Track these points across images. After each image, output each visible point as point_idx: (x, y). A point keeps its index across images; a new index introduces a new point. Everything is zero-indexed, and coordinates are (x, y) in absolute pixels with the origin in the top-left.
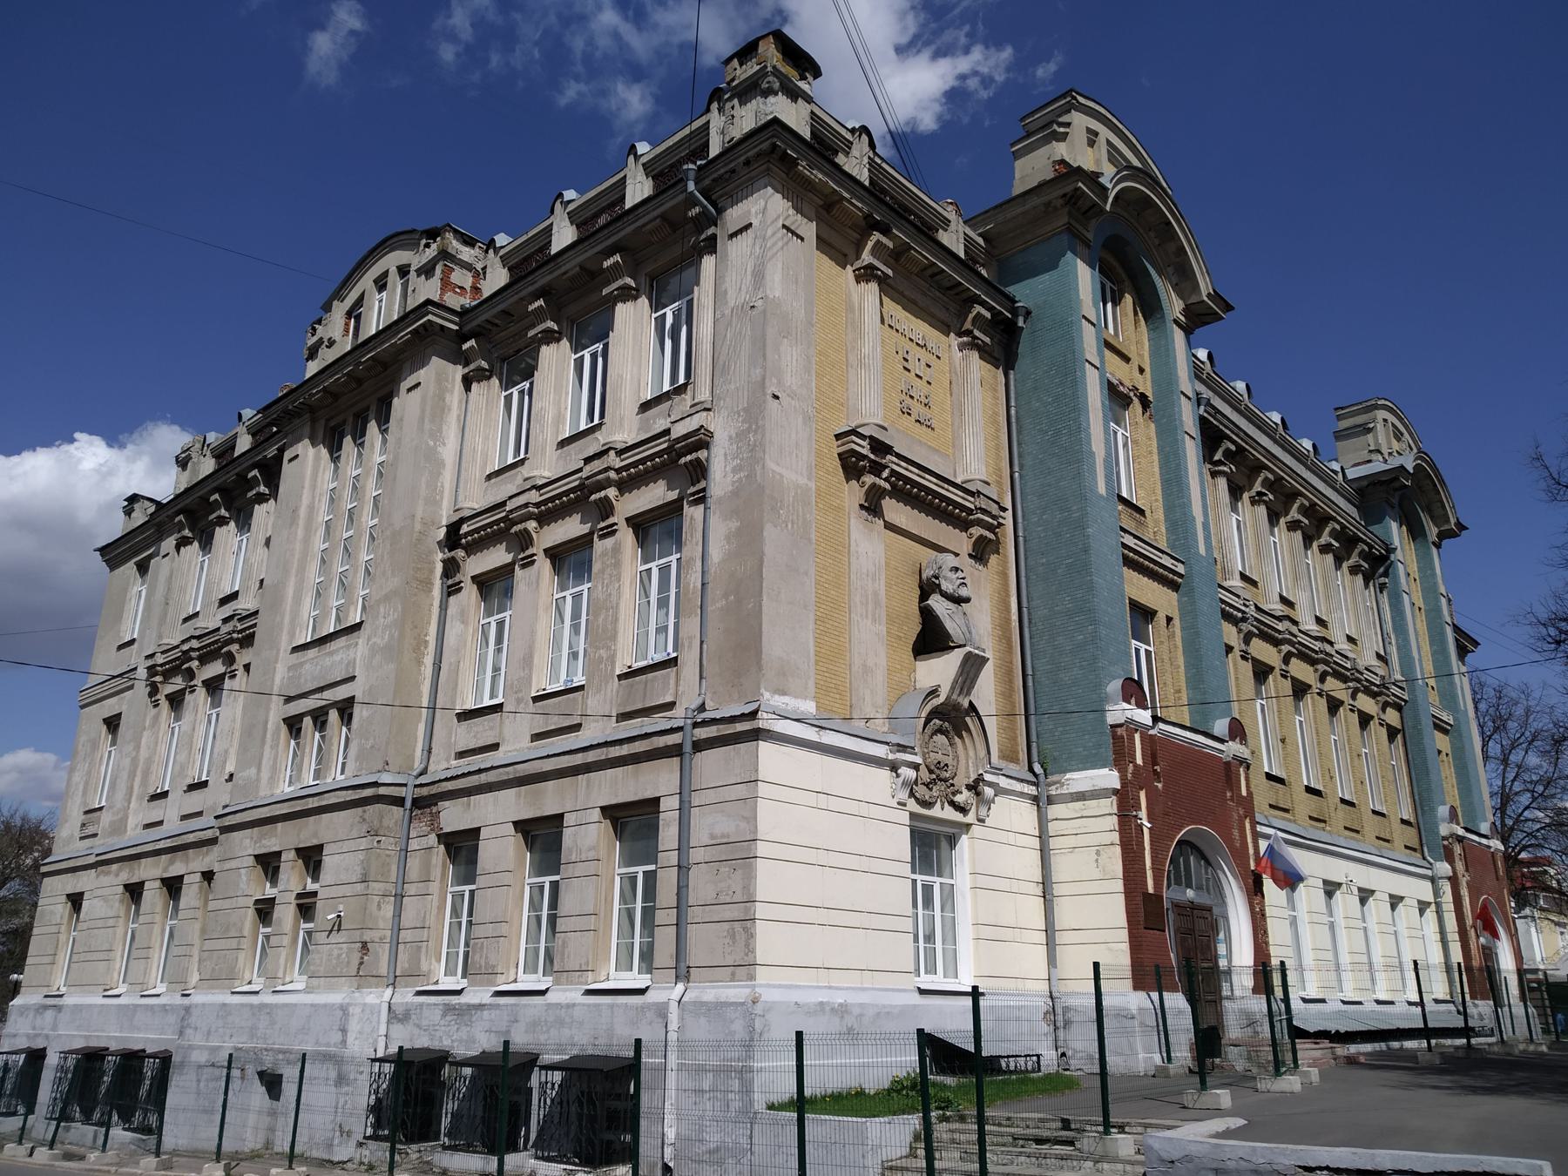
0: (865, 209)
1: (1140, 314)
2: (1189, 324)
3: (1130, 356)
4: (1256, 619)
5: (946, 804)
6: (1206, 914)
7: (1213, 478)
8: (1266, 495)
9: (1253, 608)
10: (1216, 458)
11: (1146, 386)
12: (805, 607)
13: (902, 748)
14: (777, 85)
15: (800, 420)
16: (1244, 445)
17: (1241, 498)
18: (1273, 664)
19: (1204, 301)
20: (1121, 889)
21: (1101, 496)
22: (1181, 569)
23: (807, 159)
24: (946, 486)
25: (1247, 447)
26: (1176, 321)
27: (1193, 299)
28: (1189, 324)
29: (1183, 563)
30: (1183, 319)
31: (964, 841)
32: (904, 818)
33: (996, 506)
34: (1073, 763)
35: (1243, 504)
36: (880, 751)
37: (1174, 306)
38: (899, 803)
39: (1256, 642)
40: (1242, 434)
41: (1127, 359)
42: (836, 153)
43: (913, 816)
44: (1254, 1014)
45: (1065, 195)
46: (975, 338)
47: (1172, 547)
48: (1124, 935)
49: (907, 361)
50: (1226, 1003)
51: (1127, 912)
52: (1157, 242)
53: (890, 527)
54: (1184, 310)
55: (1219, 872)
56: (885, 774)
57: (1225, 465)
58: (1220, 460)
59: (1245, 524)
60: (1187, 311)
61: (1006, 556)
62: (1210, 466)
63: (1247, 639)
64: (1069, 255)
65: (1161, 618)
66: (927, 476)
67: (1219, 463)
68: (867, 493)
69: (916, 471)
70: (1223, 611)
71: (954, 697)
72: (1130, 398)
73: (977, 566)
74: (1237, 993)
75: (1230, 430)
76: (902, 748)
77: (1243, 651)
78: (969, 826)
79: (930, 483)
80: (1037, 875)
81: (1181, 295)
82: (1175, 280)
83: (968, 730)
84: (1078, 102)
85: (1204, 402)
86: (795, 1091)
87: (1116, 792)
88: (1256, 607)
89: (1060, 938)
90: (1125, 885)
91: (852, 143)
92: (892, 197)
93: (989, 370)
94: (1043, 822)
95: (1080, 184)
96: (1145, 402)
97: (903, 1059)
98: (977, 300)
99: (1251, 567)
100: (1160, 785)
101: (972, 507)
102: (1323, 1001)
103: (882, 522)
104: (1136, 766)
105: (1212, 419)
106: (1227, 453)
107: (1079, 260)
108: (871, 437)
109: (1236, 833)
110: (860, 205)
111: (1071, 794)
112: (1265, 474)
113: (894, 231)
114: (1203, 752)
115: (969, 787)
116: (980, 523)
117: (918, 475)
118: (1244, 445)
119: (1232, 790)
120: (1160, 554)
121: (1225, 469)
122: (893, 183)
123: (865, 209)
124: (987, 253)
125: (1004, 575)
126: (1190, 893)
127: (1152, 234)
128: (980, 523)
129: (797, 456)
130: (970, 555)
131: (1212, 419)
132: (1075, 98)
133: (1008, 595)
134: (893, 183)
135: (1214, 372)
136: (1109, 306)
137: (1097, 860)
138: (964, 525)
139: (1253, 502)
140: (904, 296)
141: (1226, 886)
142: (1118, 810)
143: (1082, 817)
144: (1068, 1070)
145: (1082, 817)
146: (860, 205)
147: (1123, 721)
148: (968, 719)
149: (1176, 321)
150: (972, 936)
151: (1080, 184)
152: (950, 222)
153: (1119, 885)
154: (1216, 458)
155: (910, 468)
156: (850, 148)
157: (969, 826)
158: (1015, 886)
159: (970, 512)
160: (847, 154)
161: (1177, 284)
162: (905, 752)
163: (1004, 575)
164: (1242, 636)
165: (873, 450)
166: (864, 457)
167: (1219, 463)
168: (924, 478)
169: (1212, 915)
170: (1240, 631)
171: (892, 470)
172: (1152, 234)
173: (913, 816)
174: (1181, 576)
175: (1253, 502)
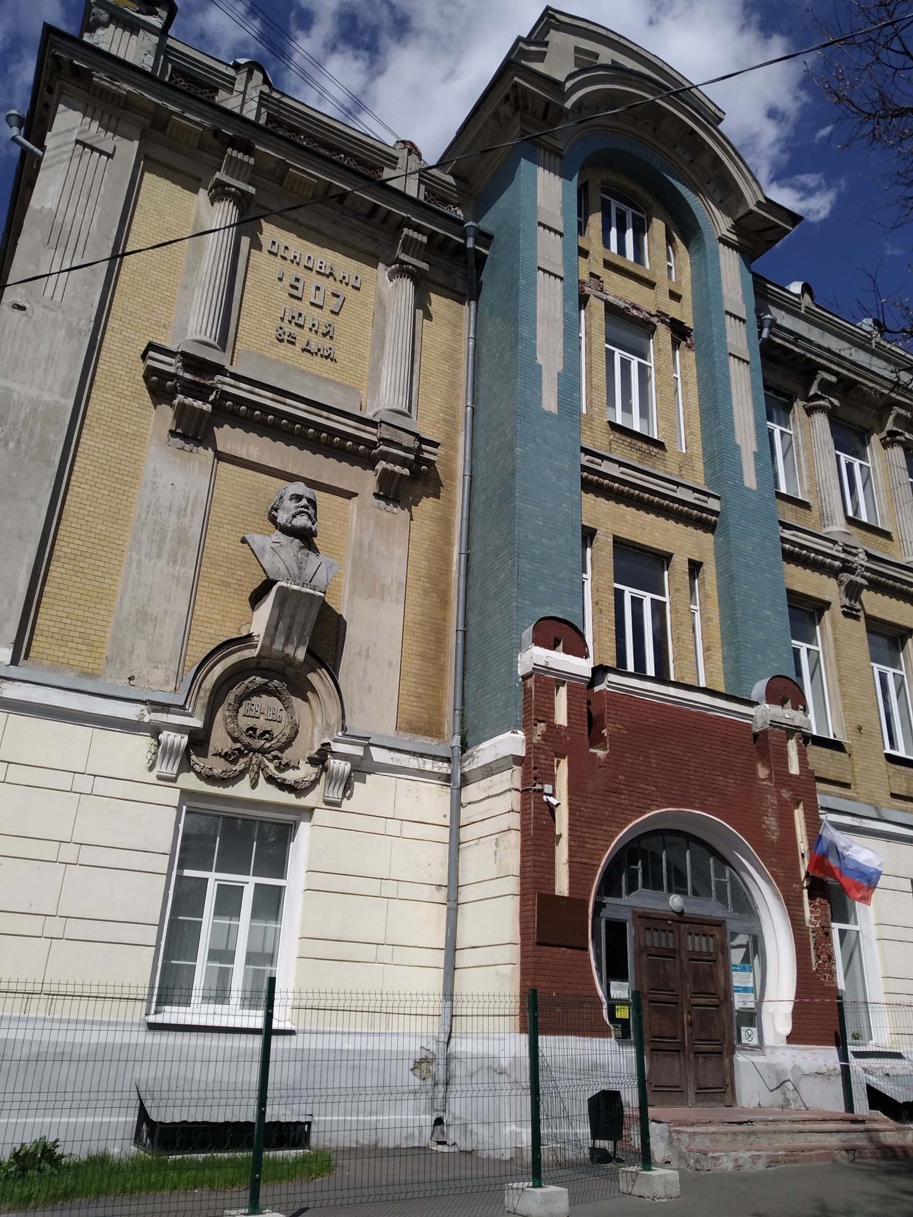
0: (207, 124)
1: (678, 240)
2: (746, 243)
3: (655, 280)
4: (868, 569)
5: (262, 779)
6: (715, 930)
7: (809, 415)
8: (901, 434)
9: (862, 556)
10: (812, 393)
11: (684, 313)
12: (20, 537)
13: (164, 707)
14: (105, 17)
15: (62, 333)
16: (853, 376)
17: (869, 441)
18: (827, 598)
19: (751, 212)
20: (516, 889)
21: (549, 414)
22: (714, 504)
23: (104, 70)
24: (325, 414)
25: (859, 379)
26: (723, 240)
27: (741, 212)
28: (746, 243)
29: (718, 498)
30: (735, 237)
31: (304, 830)
32: (172, 796)
33: (412, 438)
34: (487, 729)
35: (871, 450)
36: (130, 712)
37: (723, 224)
38: (160, 778)
39: (866, 595)
40: (847, 364)
41: (651, 285)
42: (216, 90)
43: (186, 794)
44: (784, 1072)
45: (507, 98)
46: (403, 263)
47: (708, 483)
48: (513, 954)
49: (297, 288)
50: (741, 1058)
51: (521, 923)
52: (687, 158)
53: (220, 456)
54: (733, 227)
55: (743, 874)
56: (142, 743)
57: (824, 399)
58: (816, 395)
59: (874, 469)
60: (737, 227)
61: (451, 503)
62: (804, 403)
63: (853, 591)
64: (524, 163)
65: (680, 564)
66: (288, 401)
67: (816, 397)
68: (380, 481)
69: (270, 395)
70: (784, 550)
71: (278, 646)
72: (652, 323)
73: (389, 508)
74: (768, 1040)
75: (826, 359)
76: (164, 707)
77: (845, 606)
78: (311, 810)
79: (265, 398)
80: (441, 875)
81: (727, 211)
82: (718, 198)
83: (314, 691)
84: (558, 20)
85: (767, 323)
86: (530, 1144)
87: (517, 760)
88: (868, 554)
89: (463, 958)
90: (522, 884)
91: (235, 79)
92: (308, 136)
93: (447, 305)
94: (457, 805)
95: (516, 79)
96: (679, 332)
97: (398, 1117)
98: (406, 223)
99: (882, 517)
100: (601, 753)
101: (375, 439)
102: (898, 1056)
103: (210, 452)
104: (552, 726)
105: (792, 347)
106: (826, 386)
107: (540, 170)
108: (183, 354)
109: (771, 822)
110: (198, 119)
111: (480, 767)
112: (897, 410)
113: (257, 147)
114: (711, 717)
115: (312, 761)
116: (385, 456)
117: (272, 399)
118: (853, 376)
119: (767, 765)
120: (705, 498)
121: (822, 403)
122: (373, 152)
123: (207, 124)
124: (460, 190)
125: (445, 522)
126: (676, 901)
127: (679, 150)
128: (385, 456)
129: (46, 370)
130: (376, 495)
131: (792, 347)
132: (554, 17)
133: (449, 543)
134: (373, 152)
135: (817, 306)
136: (629, 234)
137: (495, 852)
138: (368, 462)
139: (885, 445)
140: (301, 224)
141: (755, 893)
142: (523, 784)
143: (489, 797)
144: (444, 1143)
145: (489, 797)
146: (198, 119)
147: (531, 670)
148: (313, 677)
149: (723, 240)
150: (296, 953)
151: (516, 79)
152: (397, 159)
153: (513, 885)
154: (812, 393)
155: (257, 390)
156: (233, 84)
157: (311, 810)
158: (406, 891)
159: (371, 445)
160: (231, 91)
161: (721, 201)
162: (168, 713)
163: (445, 522)
164: (843, 588)
165: (186, 367)
166: (173, 376)
167: (816, 397)
168: (285, 404)
169: (724, 932)
170: (840, 583)
171: (224, 392)
172: (679, 150)
173: (186, 794)
174: (715, 513)
175: (885, 445)
